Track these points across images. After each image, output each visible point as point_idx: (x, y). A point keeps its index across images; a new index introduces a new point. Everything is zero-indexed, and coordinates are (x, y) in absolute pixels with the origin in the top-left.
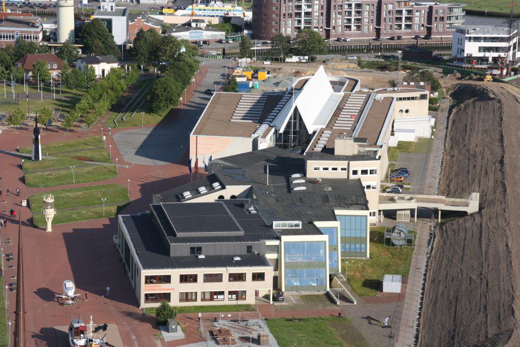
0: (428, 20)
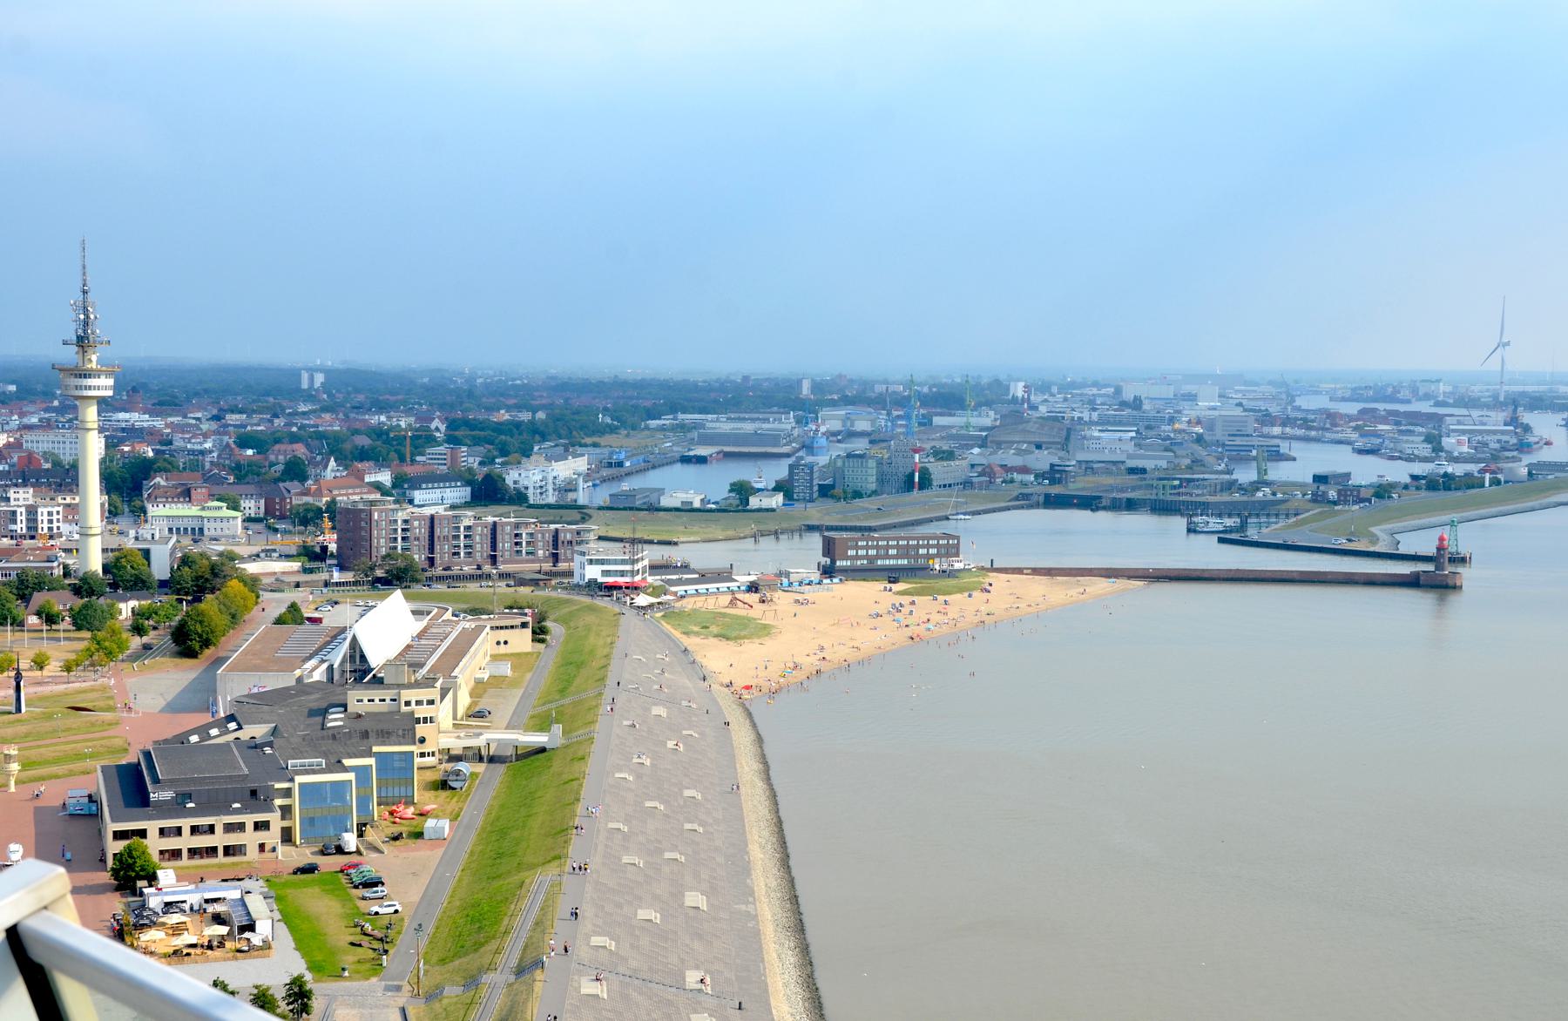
0: (553, 545)
